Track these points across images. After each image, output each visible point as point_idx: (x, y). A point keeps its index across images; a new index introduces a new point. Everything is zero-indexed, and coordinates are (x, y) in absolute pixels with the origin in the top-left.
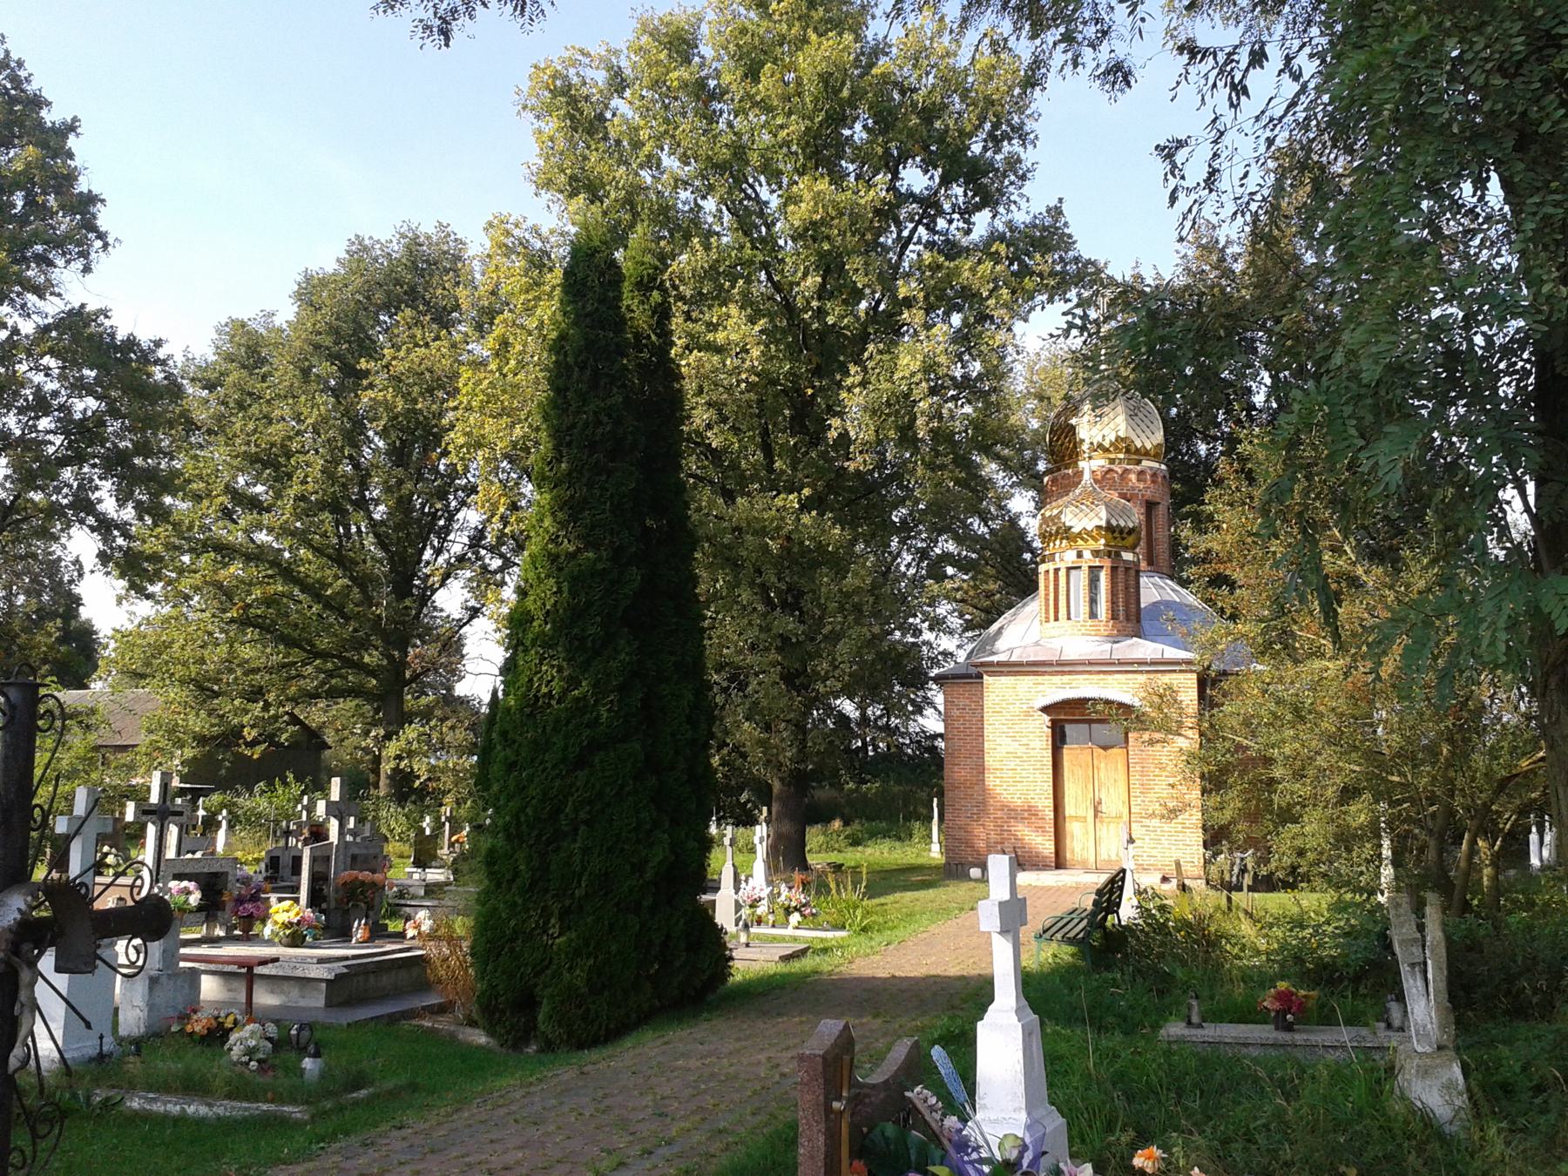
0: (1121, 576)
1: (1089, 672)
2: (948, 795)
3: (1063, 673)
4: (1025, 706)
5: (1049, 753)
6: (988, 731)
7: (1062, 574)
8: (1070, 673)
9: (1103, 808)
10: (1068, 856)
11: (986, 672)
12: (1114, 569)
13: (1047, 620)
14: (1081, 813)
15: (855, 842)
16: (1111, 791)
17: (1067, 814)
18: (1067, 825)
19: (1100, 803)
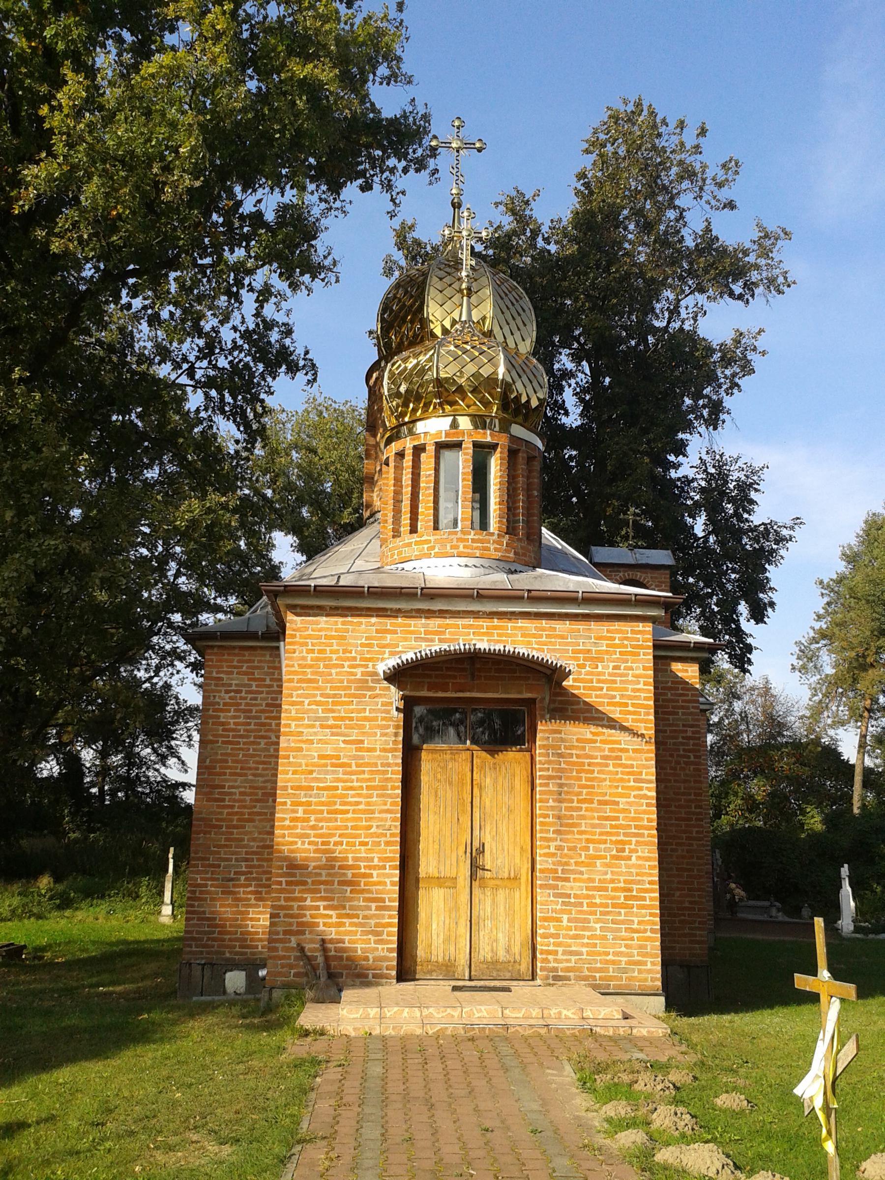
0: (521, 467)
1: (476, 615)
2: (198, 840)
3: (429, 614)
4: (359, 671)
5: (396, 759)
6: (289, 712)
7: (427, 460)
8: (442, 614)
9: (487, 861)
10: (421, 953)
11: (292, 608)
12: (512, 454)
13: (396, 534)
14: (447, 871)
15: (65, 903)
16: (503, 828)
17: (422, 874)
18: (421, 892)
19: (481, 851)
